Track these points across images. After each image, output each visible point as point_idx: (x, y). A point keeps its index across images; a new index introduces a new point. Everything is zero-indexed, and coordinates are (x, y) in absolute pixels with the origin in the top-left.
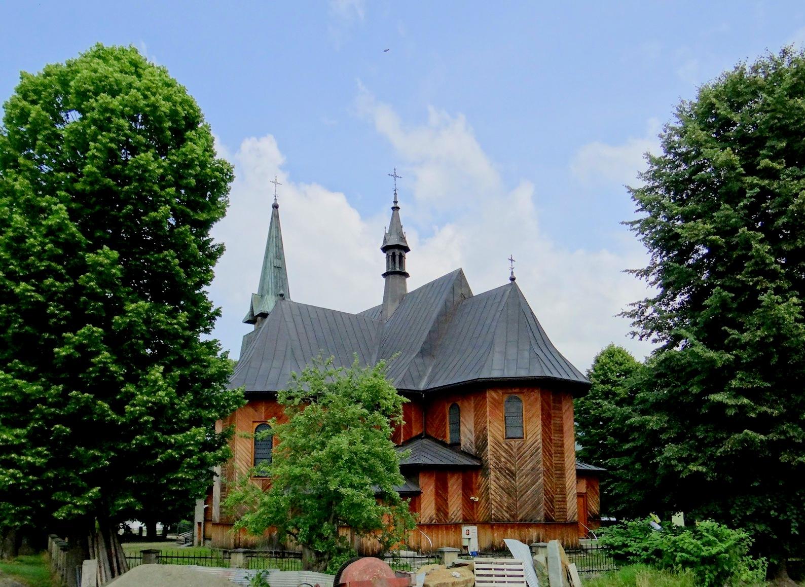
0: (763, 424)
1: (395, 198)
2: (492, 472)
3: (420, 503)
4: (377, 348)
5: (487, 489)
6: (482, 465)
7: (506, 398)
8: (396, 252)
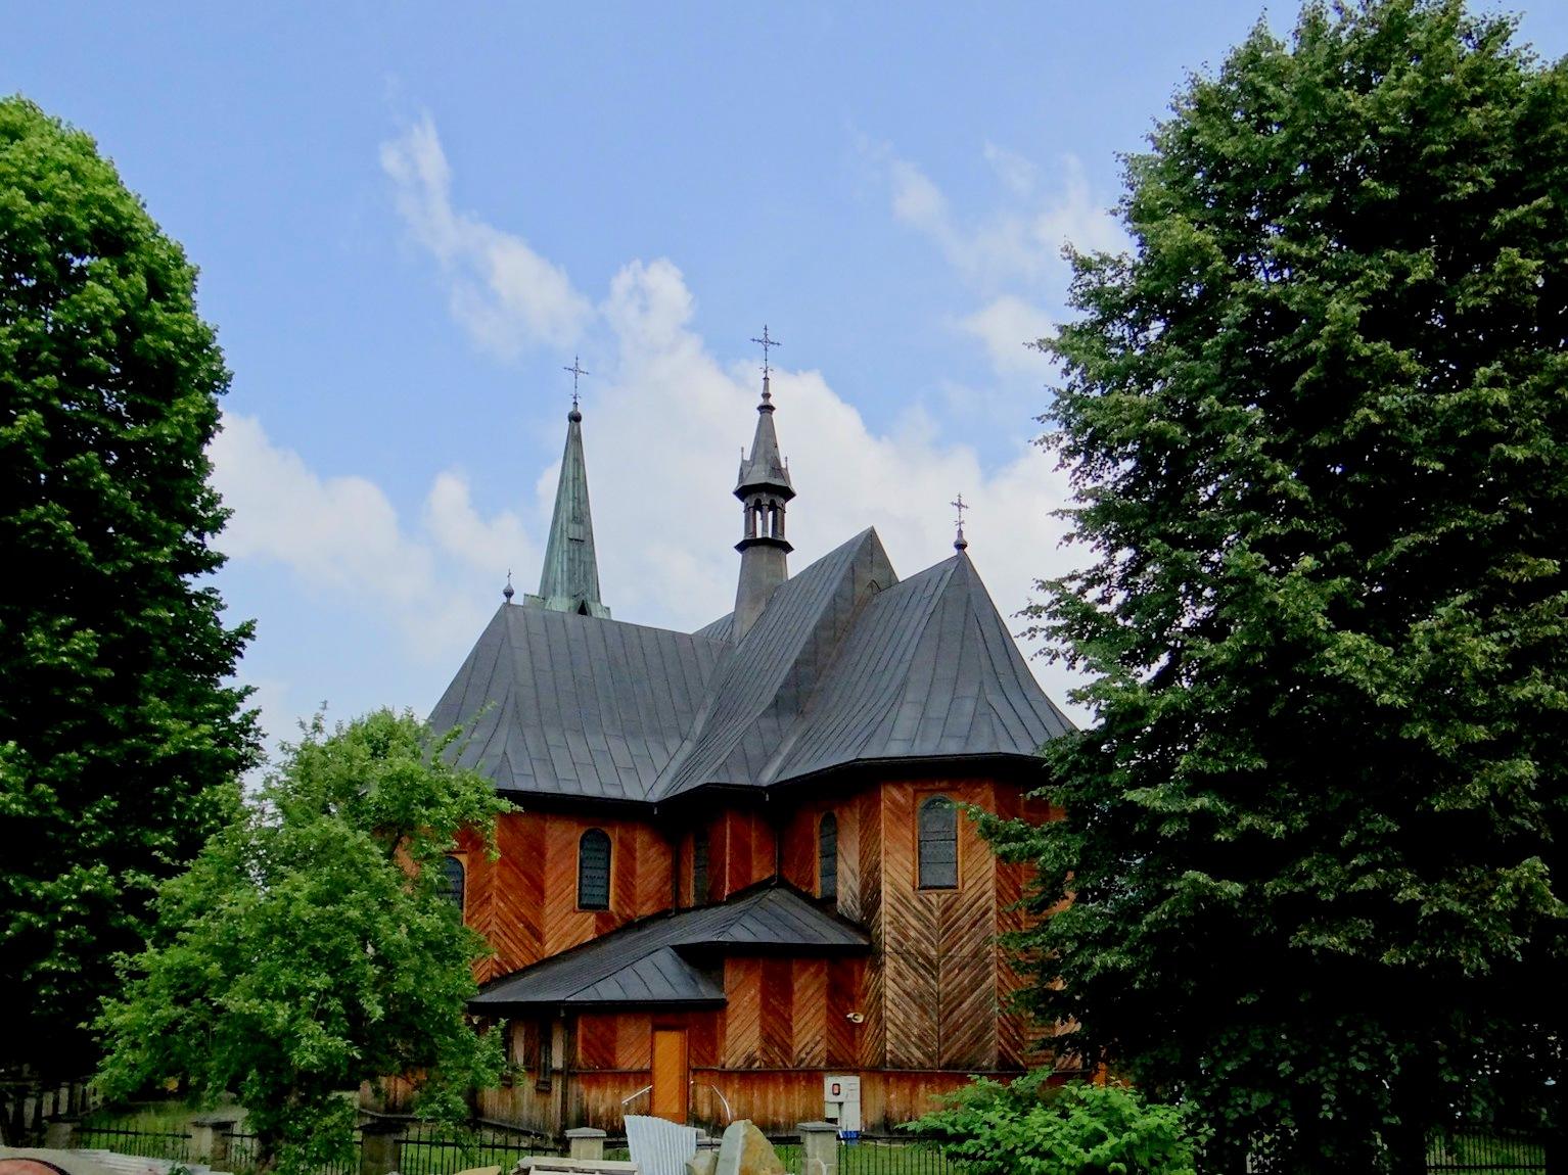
0: (1251, 858)
1: (766, 386)
2: (888, 960)
3: (724, 1026)
4: (710, 701)
5: (880, 996)
6: (871, 943)
7: (921, 802)
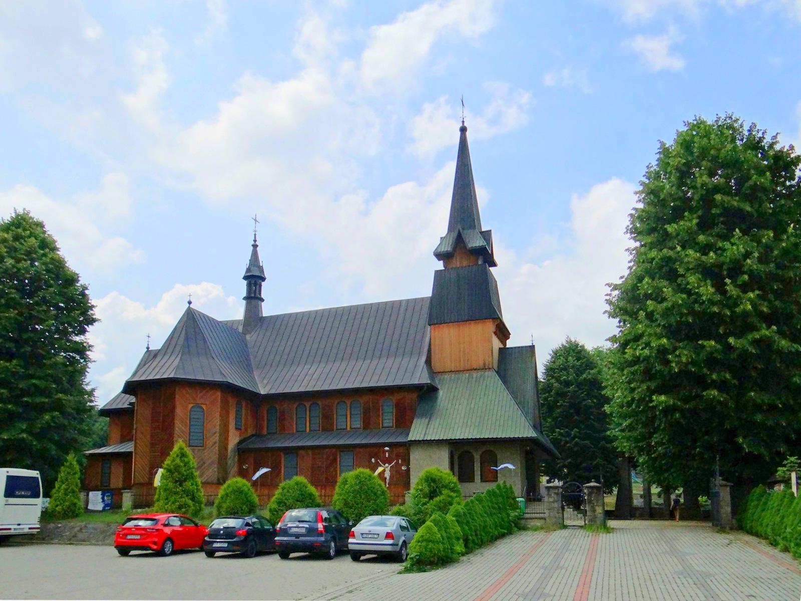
1: (255, 237)
8: (255, 280)
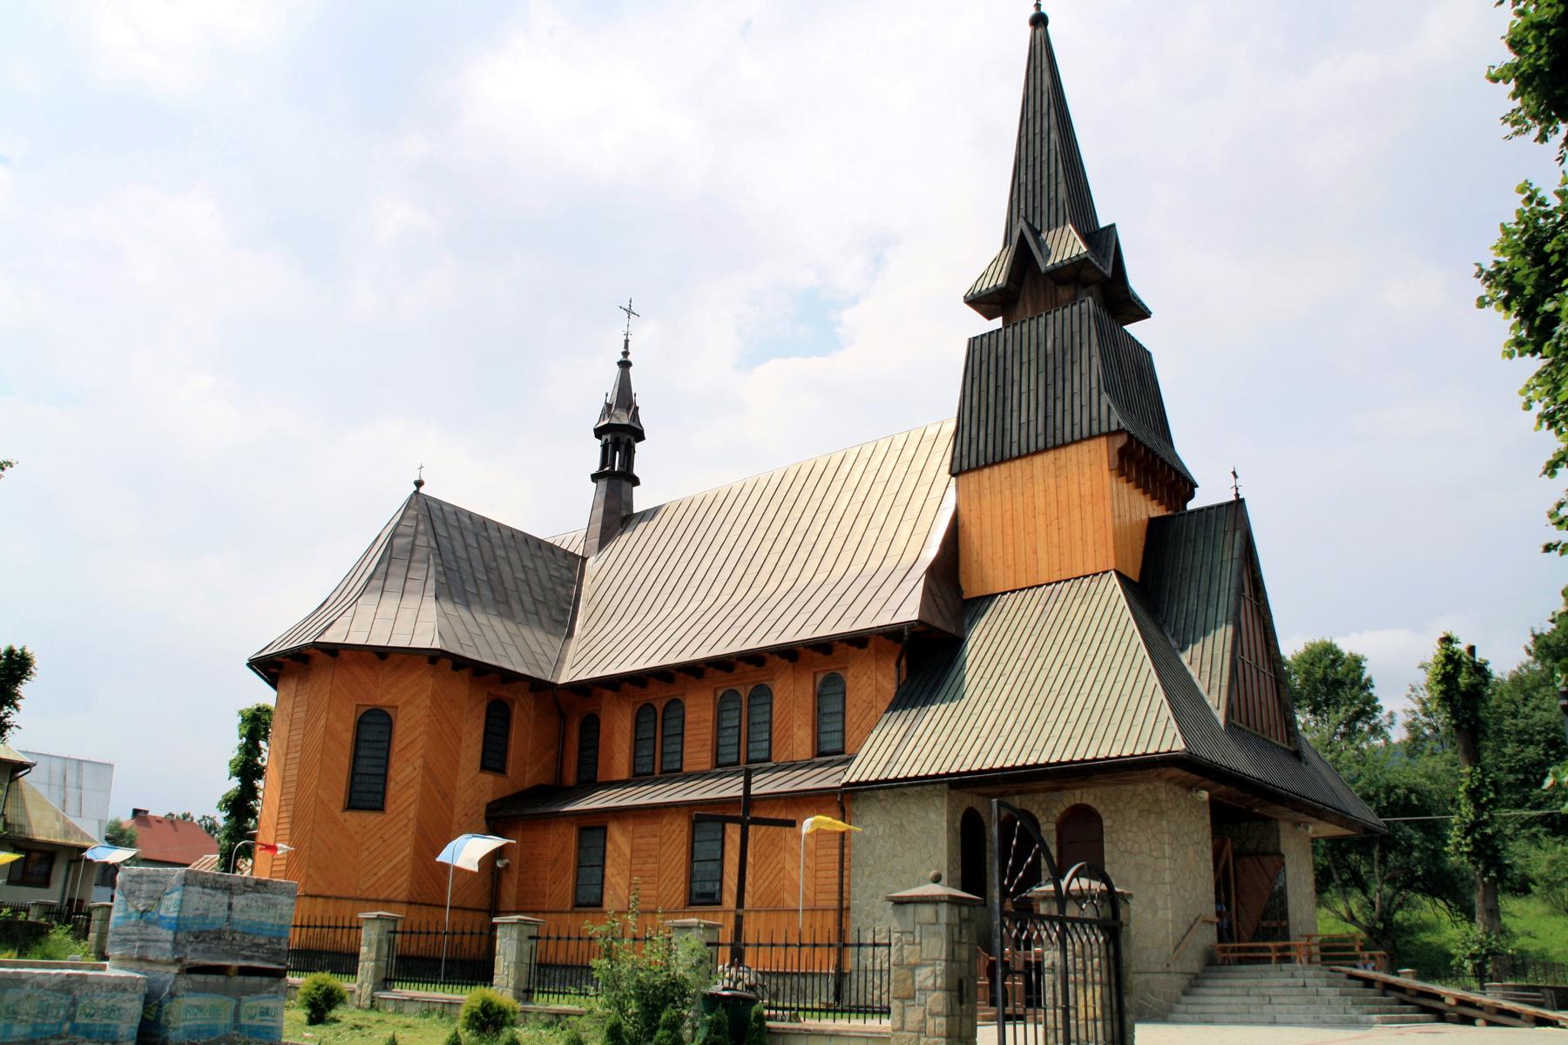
1: (626, 346)
